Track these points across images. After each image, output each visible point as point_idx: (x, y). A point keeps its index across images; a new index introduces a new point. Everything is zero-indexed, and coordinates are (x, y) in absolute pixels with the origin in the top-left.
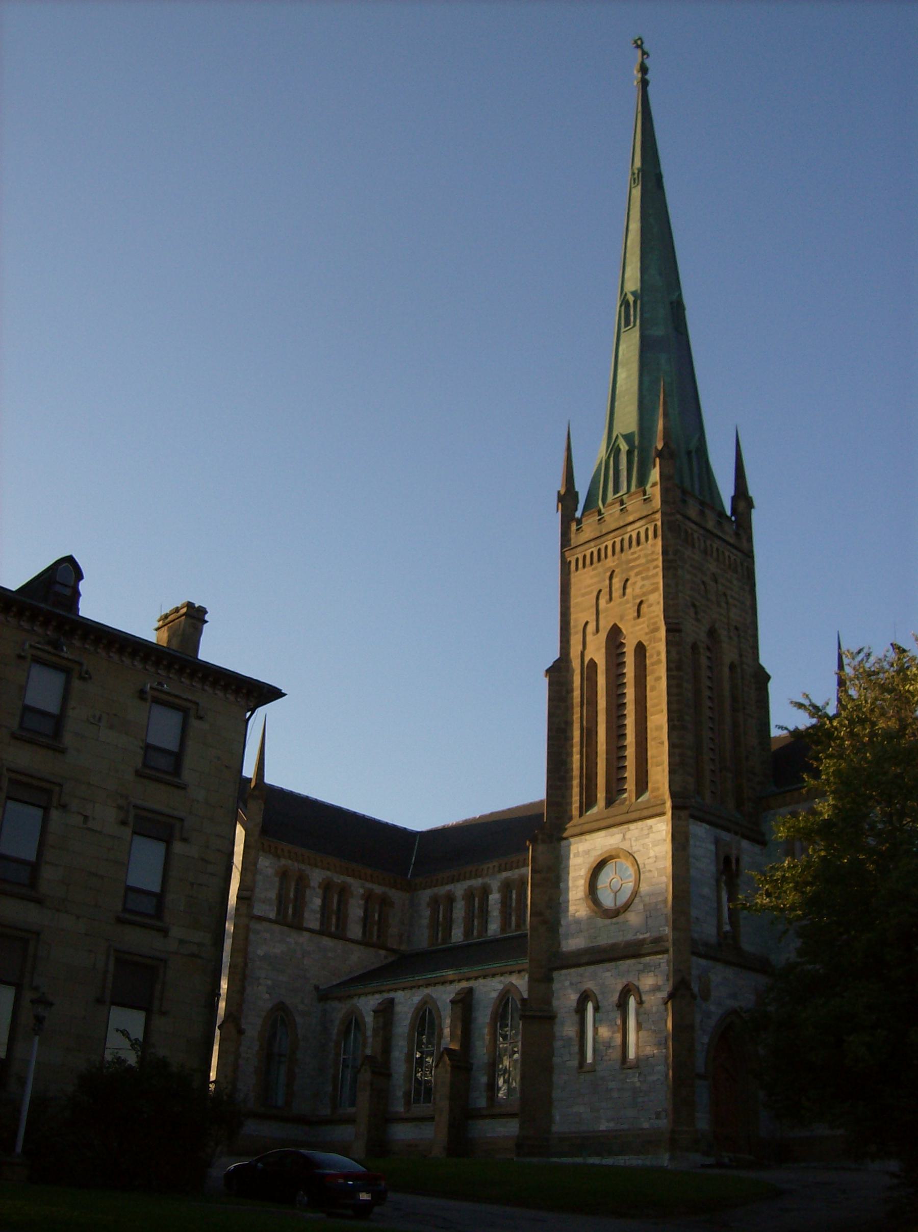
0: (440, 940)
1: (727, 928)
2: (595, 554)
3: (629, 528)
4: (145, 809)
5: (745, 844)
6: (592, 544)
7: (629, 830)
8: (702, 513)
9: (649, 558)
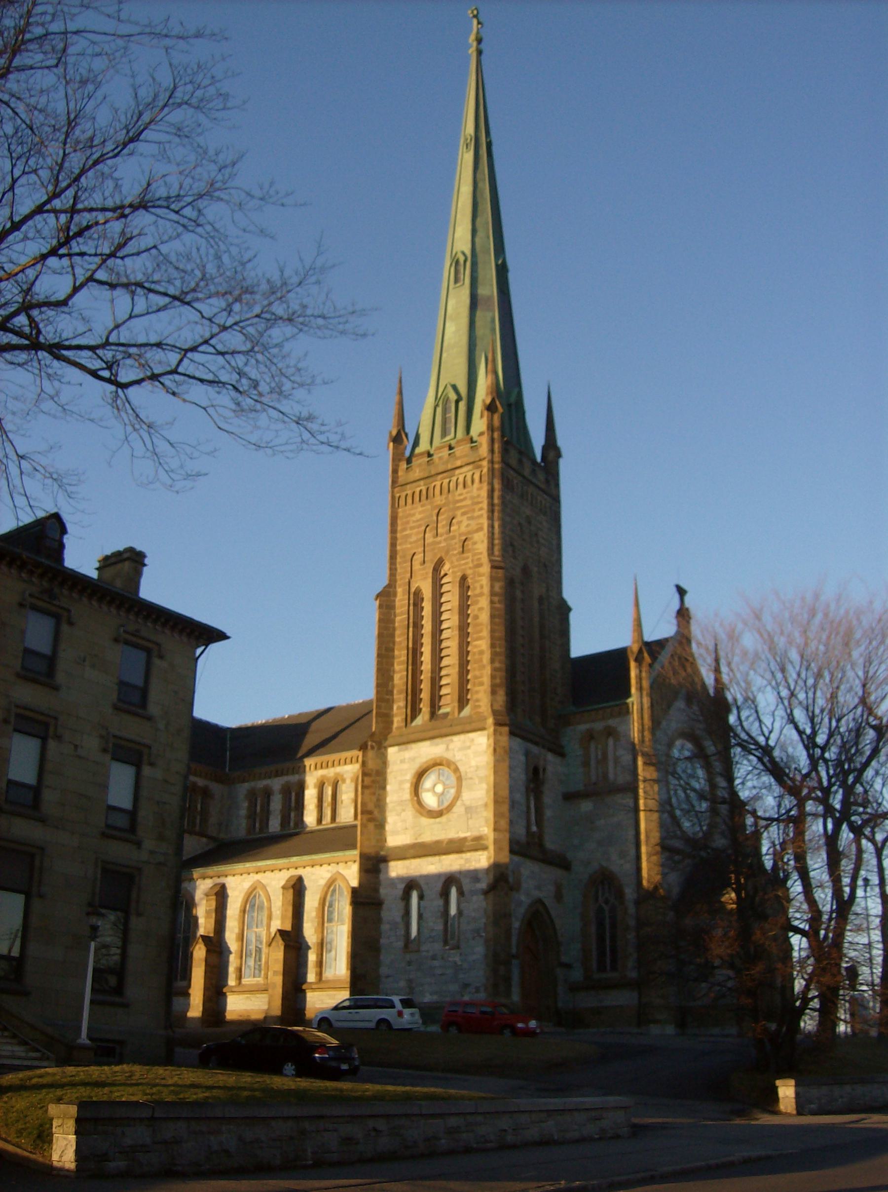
0: (257, 830)
1: (534, 828)
2: (424, 492)
3: (457, 472)
4: (121, 738)
5: (550, 756)
6: (422, 483)
7: (452, 741)
8: (520, 462)
9: (476, 500)
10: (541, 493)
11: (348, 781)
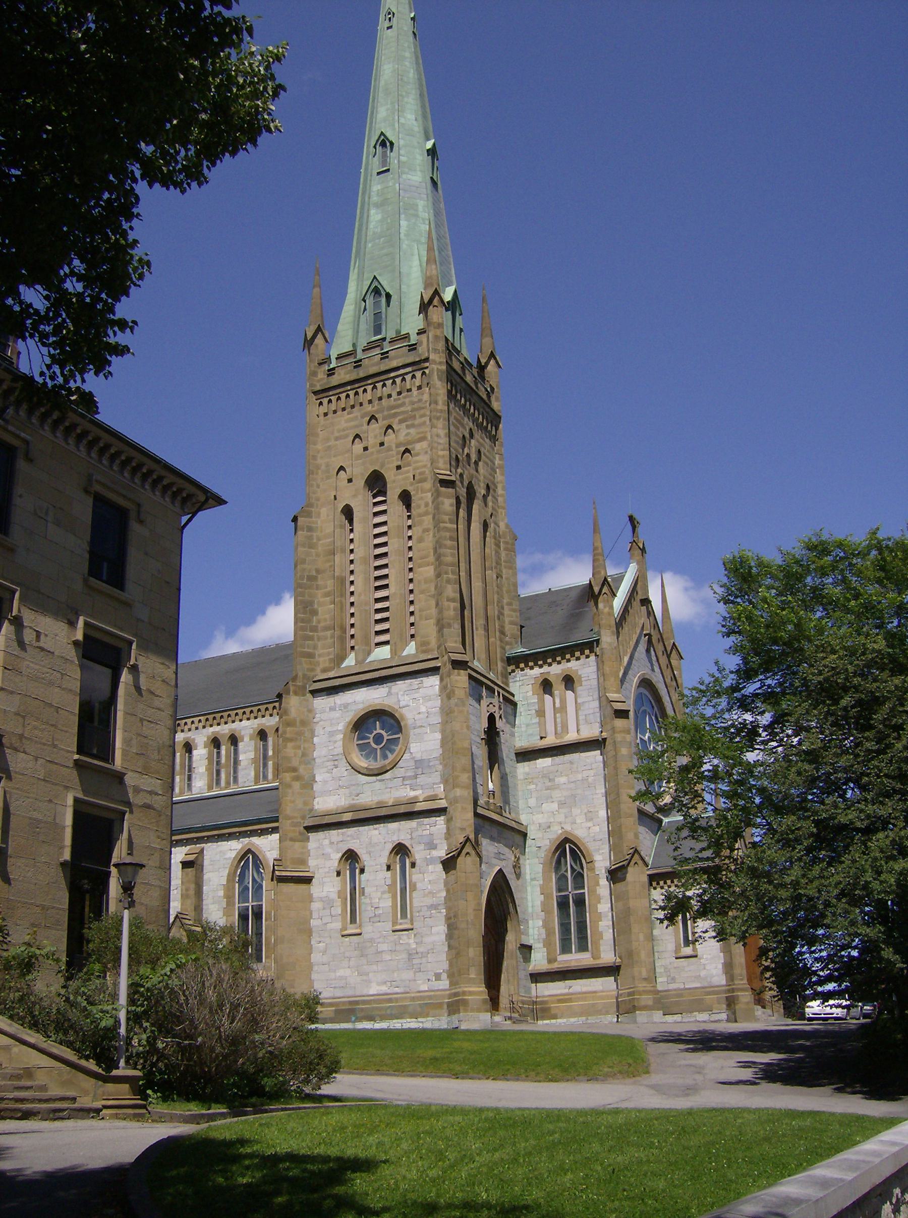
9: (416, 406)
10: (483, 404)
11: (246, 739)
